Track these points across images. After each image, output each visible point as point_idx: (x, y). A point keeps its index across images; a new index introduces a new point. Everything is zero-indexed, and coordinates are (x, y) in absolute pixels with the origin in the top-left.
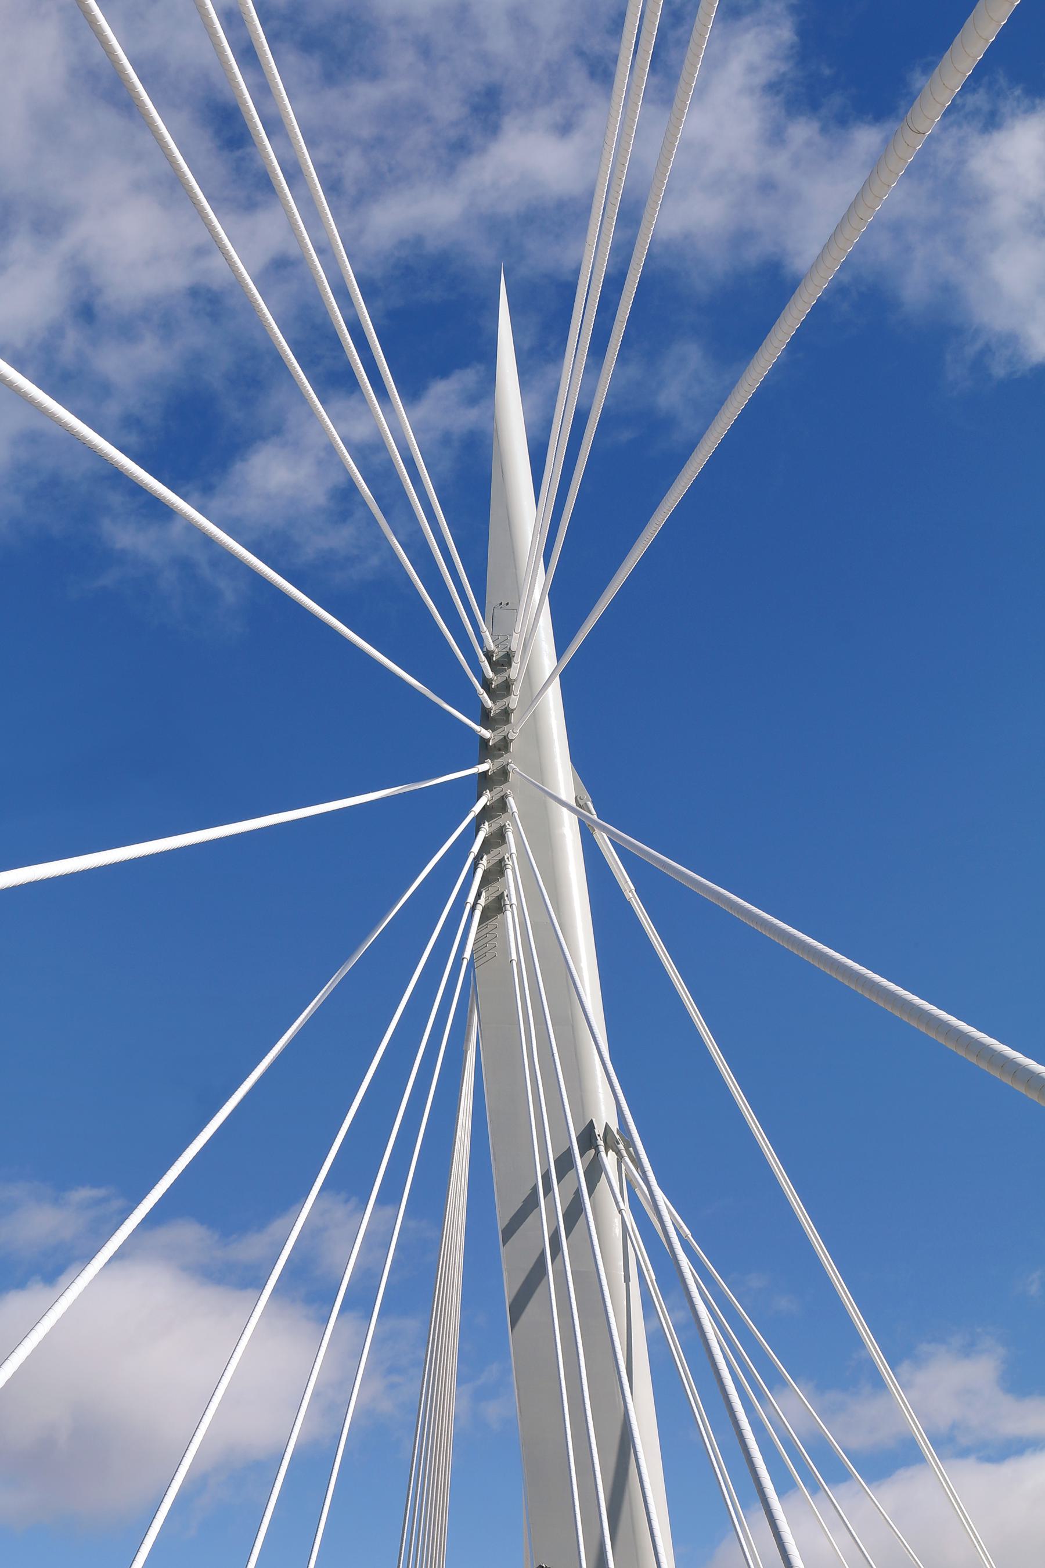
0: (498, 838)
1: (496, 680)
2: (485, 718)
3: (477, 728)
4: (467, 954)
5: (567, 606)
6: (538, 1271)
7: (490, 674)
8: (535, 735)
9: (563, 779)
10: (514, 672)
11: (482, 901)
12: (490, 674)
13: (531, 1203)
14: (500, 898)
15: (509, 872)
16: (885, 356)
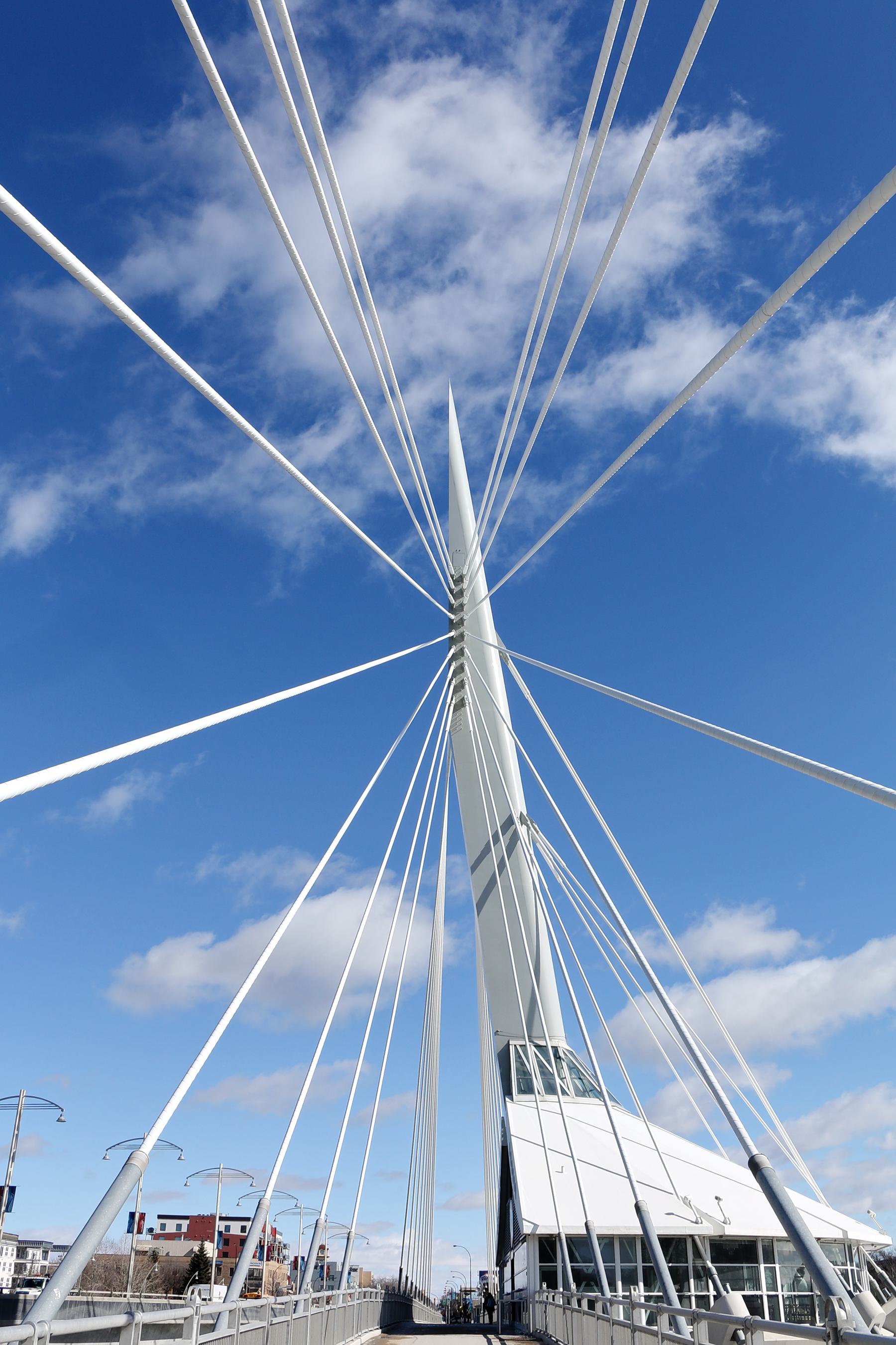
0: (460, 669)
1: (456, 589)
2: (451, 608)
3: (449, 614)
4: (448, 729)
5: (493, 574)
6: (492, 882)
7: (453, 586)
8: (477, 618)
9: (491, 634)
10: (465, 585)
11: (454, 702)
12: (453, 586)
13: (487, 850)
14: (463, 699)
15: (467, 687)
16: (744, 482)
